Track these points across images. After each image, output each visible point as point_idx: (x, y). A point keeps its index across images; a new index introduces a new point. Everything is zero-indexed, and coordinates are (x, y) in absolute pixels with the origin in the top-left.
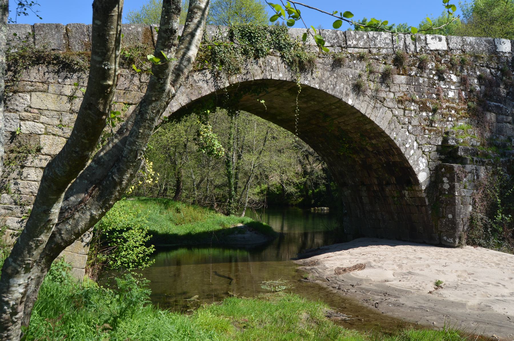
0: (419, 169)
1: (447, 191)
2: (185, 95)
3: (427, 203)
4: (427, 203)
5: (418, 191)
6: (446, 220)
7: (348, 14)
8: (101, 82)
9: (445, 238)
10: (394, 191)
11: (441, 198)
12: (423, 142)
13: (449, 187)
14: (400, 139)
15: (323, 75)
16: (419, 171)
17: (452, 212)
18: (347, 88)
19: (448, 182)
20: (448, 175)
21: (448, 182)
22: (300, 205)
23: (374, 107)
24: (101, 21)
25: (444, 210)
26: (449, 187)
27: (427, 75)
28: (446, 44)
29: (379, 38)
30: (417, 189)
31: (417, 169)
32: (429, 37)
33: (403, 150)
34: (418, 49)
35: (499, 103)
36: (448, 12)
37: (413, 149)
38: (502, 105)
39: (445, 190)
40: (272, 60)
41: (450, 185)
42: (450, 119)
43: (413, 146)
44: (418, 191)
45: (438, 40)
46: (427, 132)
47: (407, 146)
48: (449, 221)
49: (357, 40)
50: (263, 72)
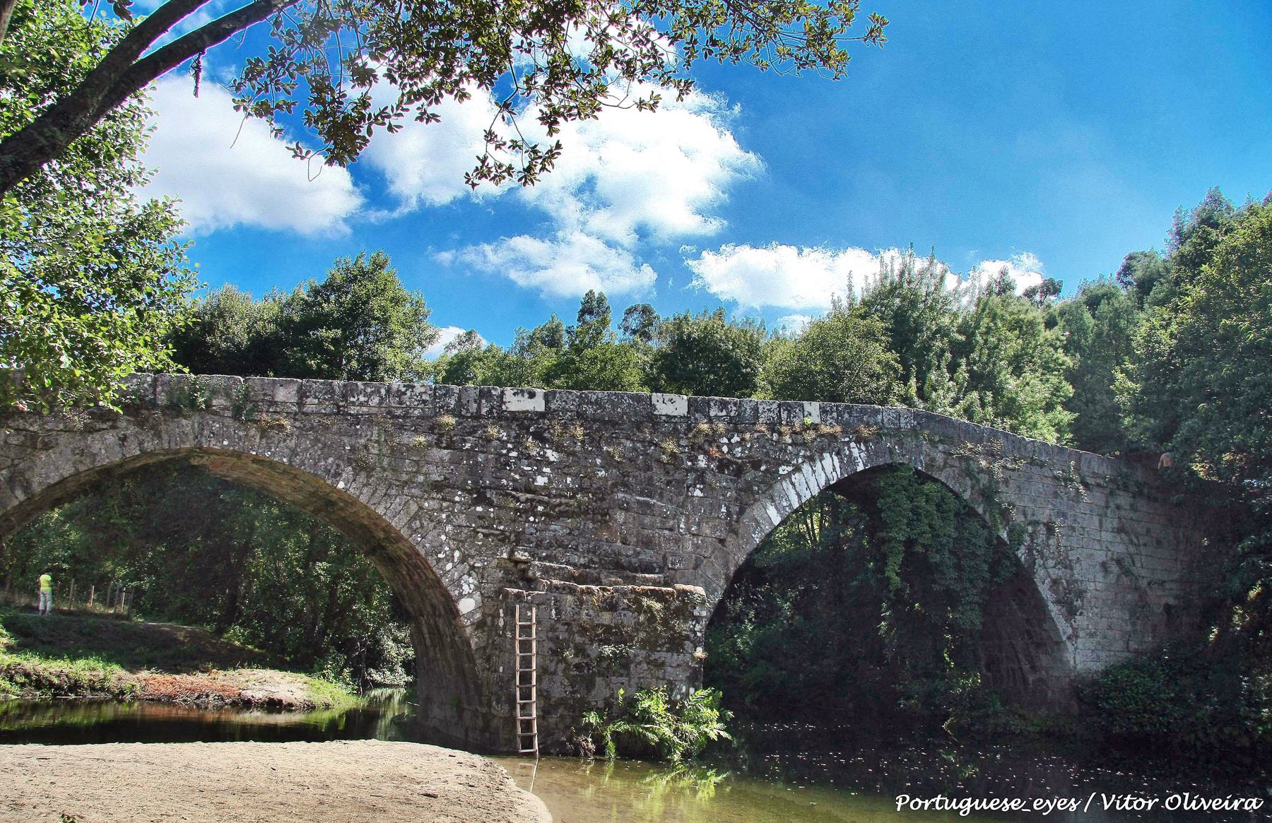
2: (70, 463)
3: (45, 579)
4: (45, 579)
7: (467, 174)
14: (428, 545)
16: (461, 596)
22: (21, 123)
27: (495, 449)
28: (543, 402)
29: (408, 393)
31: (457, 592)
32: (509, 391)
33: (431, 561)
34: (484, 411)
35: (647, 496)
37: (453, 562)
38: (653, 501)
42: (532, 519)
43: (453, 557)
45: (526, 395)
46: (480, 536)
49: (369, 396)
50: (197, 437)
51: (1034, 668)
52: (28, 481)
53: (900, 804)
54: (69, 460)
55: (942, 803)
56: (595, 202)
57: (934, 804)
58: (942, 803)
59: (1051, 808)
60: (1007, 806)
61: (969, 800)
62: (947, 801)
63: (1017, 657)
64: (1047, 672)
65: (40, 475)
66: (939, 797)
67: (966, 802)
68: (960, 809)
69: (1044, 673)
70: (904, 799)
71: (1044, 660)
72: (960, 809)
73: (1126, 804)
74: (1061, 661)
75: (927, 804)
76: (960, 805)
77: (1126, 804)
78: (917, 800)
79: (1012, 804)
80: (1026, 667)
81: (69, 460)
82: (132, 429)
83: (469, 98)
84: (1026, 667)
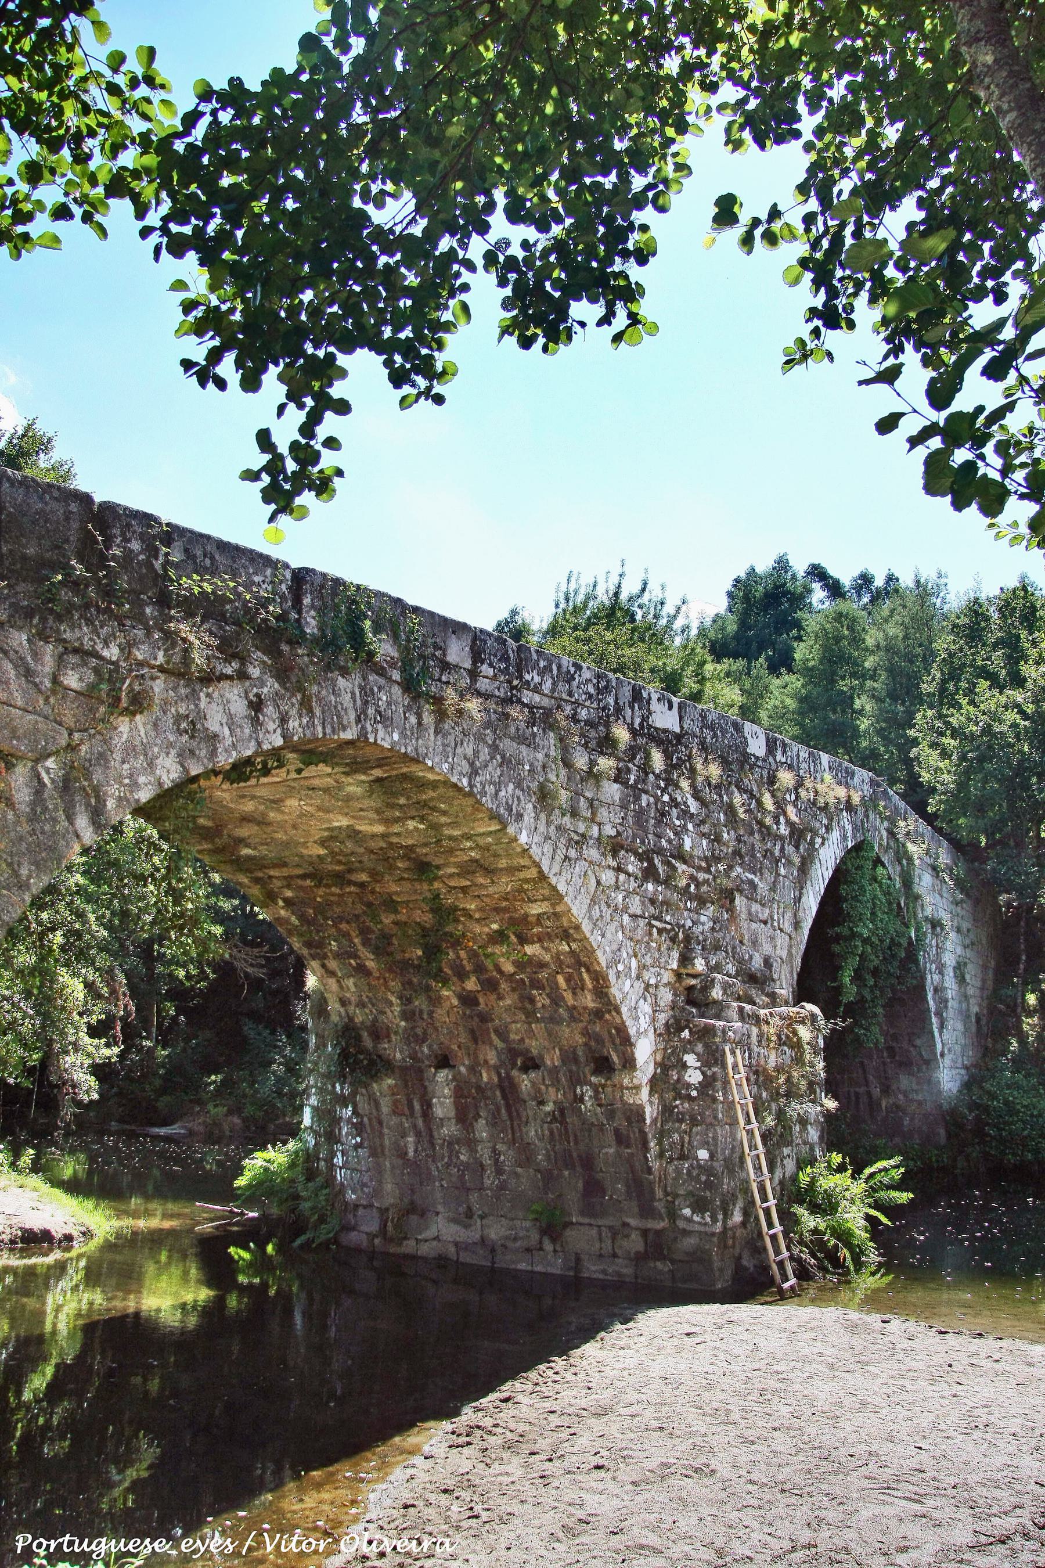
0: (638, 1031)
1: (696, 1089)
5: (627, 1088)
6: (691, 1165)
8: (274, 1240)
9: (687, 1212)
10: (547, 1086)
11: (677, 1106)
12: (648, 960)
13: (700, 1078)
15: (476, 753)
16: (639, 1034)
17: (707, 1143)
18: (519, 798)
19: (699, 1064)
20: (699, 1048)
21: (699, 1064)
23: (566, 857)
24: (239, 1188)
25: (686, 1138)
26: (700, 1078)
30: (626, 1082)
36: (368, 984)
39: (689, 1086)
40: (380, 689)
41: (703, 1073)
44: (627, 1088)
47: (620, 967)
48: (699, 1166)
51: (886, 1090)
52: (96, 790)
53: (20, 1545)
54: (171, 745)
55: (71, 1543)
56: (810, 345)
57: (61, 1544)
58: (71, 1543)
59: (202, 1550)
60: (150, 1547)
61: (104, 1540)
62: (77, 1542)
63: (866, 1079)
64: (905, 1096)
65: (119, 779)
66: (67, 1537)
67: (99, 1543)
68: (93, 1552)
69: (901, 1097)
70: (25, 1540)
71: (905, 1082)
72: (93, 1552)
73: (293, 1545)
74: (929, 1081)
75: (53, 1544)
76: (93, 1547)
77: (293, 1545)
78: (41, 1540)
79: (156, 1544)
80: (876, 1092)
81: (171, 745)
82: (271, 686)
83: (775, 205)
84: (876, 1092)
